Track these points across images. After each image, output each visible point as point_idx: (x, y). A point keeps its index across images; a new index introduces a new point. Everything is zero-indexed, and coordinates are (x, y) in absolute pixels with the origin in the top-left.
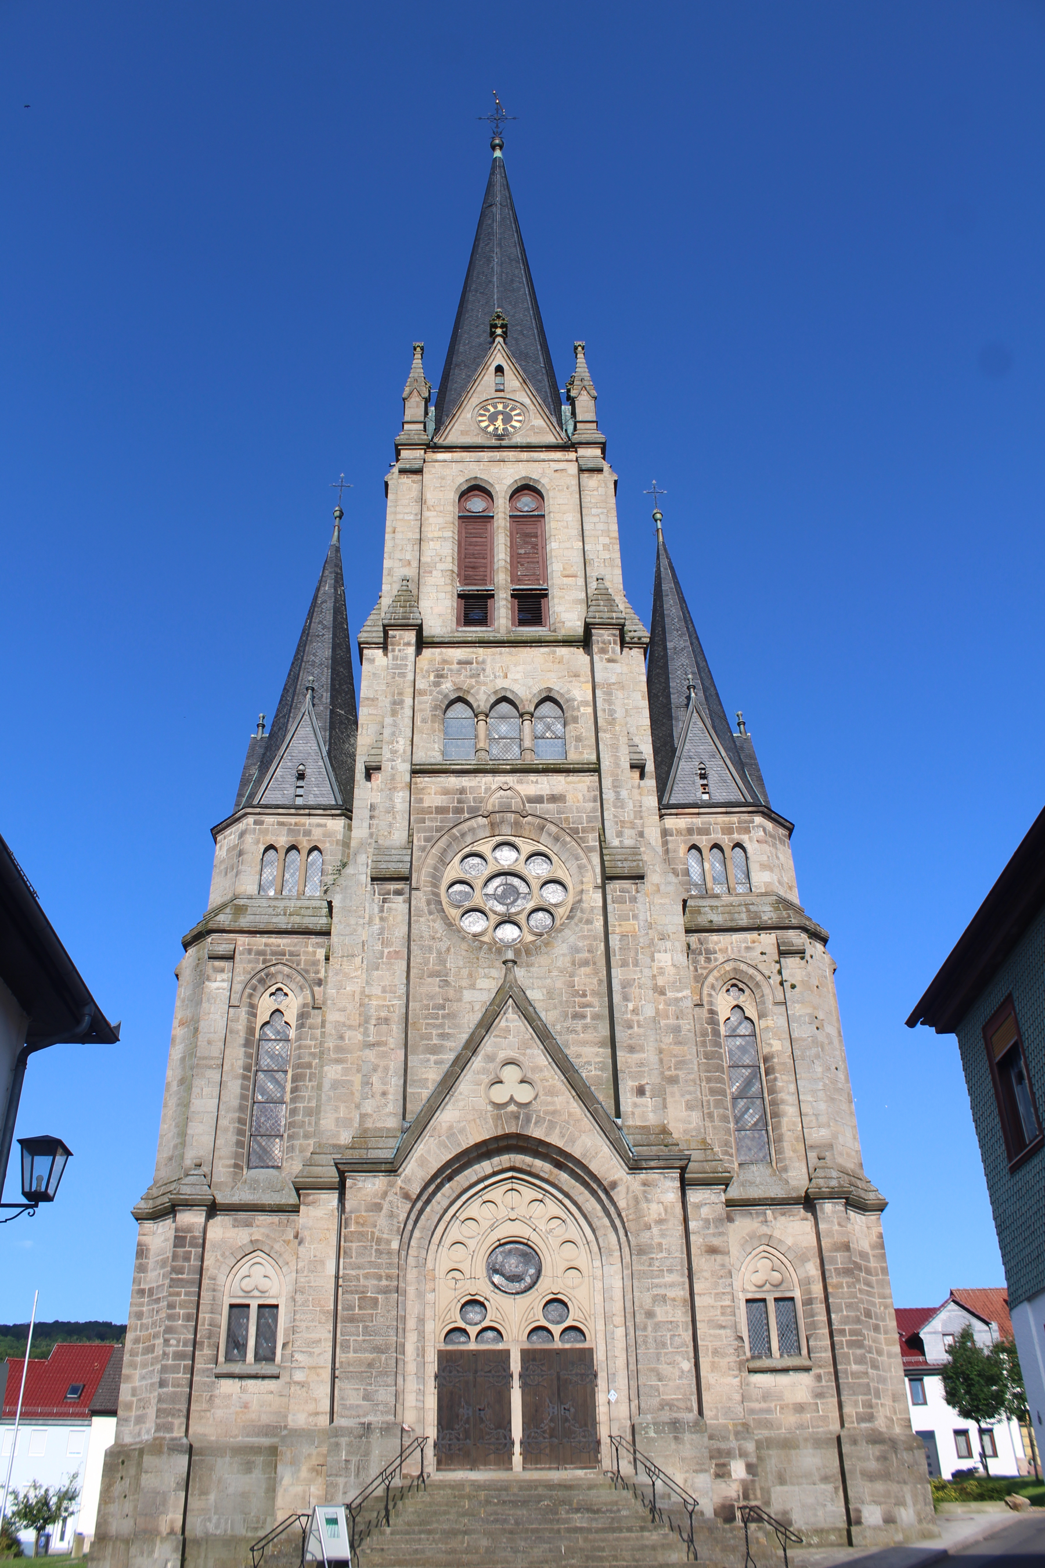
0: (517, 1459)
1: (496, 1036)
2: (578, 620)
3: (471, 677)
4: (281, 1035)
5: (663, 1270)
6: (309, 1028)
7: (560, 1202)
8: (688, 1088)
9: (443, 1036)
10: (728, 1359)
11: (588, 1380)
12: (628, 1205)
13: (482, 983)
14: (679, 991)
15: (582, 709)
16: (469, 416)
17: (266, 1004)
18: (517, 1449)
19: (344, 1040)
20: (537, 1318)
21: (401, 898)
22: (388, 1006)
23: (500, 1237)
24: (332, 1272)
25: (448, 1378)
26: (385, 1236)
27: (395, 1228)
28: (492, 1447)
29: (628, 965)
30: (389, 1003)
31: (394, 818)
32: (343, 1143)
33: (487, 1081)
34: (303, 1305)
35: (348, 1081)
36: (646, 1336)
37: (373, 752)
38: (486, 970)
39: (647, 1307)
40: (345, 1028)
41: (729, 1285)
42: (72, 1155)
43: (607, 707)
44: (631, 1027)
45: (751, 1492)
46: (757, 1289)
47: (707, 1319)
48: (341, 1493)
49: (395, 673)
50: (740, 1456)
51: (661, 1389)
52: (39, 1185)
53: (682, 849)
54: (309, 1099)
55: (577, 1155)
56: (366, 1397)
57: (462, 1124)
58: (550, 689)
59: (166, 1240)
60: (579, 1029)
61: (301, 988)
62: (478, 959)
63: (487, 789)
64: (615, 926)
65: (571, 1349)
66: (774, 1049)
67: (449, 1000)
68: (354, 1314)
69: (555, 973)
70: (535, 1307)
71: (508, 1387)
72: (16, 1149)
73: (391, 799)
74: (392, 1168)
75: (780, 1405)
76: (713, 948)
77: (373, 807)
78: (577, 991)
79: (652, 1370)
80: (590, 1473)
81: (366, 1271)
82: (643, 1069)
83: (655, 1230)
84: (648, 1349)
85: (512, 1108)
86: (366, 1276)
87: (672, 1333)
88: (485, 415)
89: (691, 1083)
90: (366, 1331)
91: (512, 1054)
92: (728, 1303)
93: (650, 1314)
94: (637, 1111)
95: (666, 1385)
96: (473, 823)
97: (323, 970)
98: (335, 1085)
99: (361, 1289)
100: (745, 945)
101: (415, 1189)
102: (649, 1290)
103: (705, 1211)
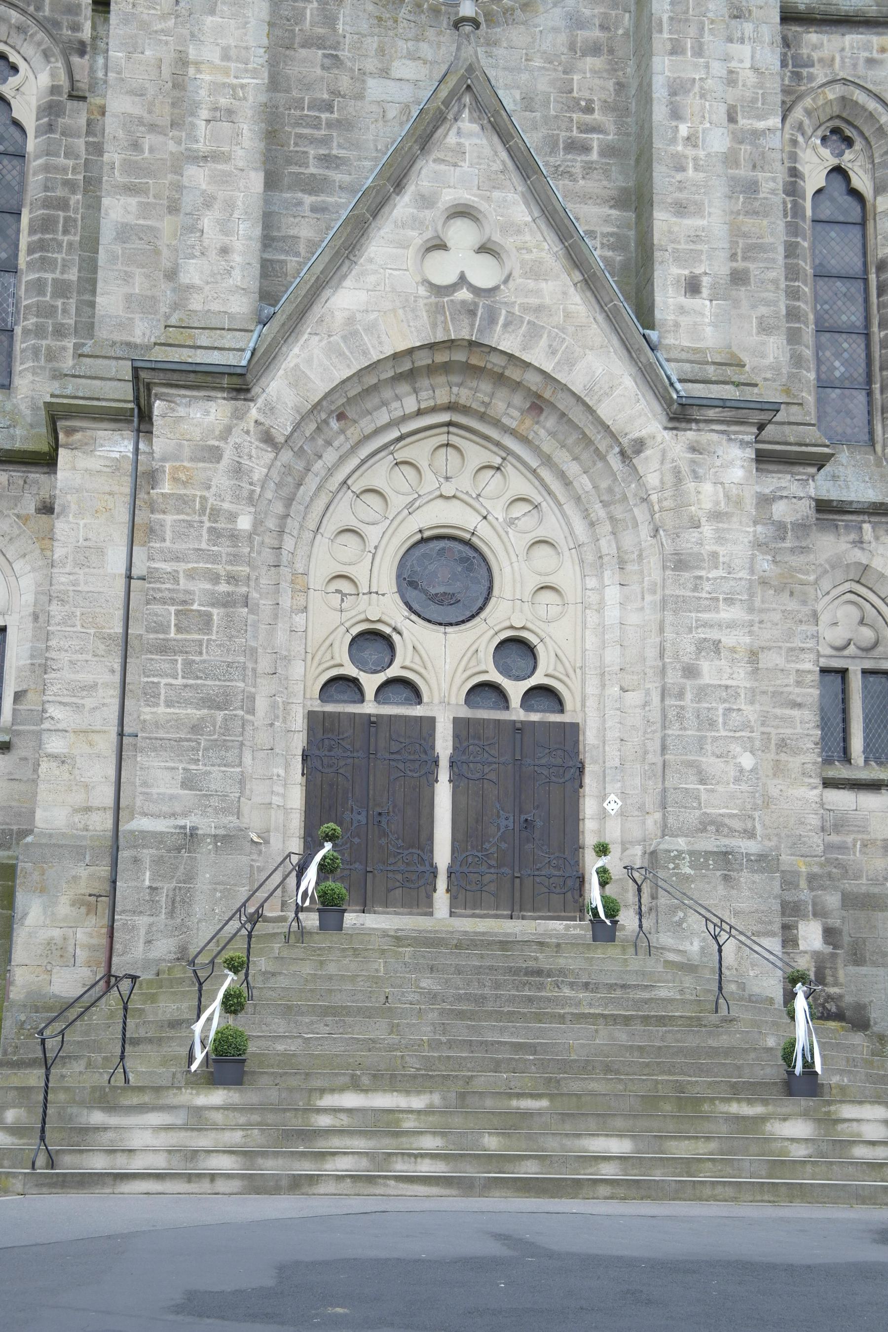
0: (441, 897)
4: (6, 143)
5: (717, 599)
6: (63, 134)
7: (534, 472)
8: (765, 295)
9: (327, 160)
10: (801, 759)
11: (567, 777)
12: (662, 482)
13: (404, 69)
14: (760, 118)
18: (442, 883)
19: (143, 152)
20: (483, 667)
22: (233, 87)
23: (422, 525)
24: (121, 569)
25: (325, 760)
26: (226, 506)
27: (245, 494)
28: (399, 877)
29: (683, 52)
30: (235, 81)
32: (138, 341)
33: (419, 241)
34: (64, 622)
35: (151, 228)
36: (682, 708)
38: (410, 43)
39: (686, 659)
40: (142, 129)
41: (813, 636)
44: (682, 169)
45: (828, 972)
46: (834, 653)
47: (771, 689)
48: (142, 941)
50: (815, 915)
51: (704, 797)
54: (64, 266)
55: (577, 389)
56: (188, 783)
57: (373, 316)
60: (577, 170)
62: (396, 21)
65: (541, 723)
67: (339, 95)
68: (167, 640)
69: (538, 63)
70: (482, 649)
75: (862, 840)
76: (809, 56)
78: (577, 101)
79: (690, 764)
80: (575, 927)
81: (190, 566)
82: (699, 247)
83: (707, 530)
84: (685, 729)
85: (464, 294)
86: (191, 575)
87: (727, 705)
89: (771, 287)
90: (189, 669)
91: (466, 196)
93: (690, 672)
94: (684, 320)
95: (713, 791)
97: (88, 26)
98: (124, 233)
99: (181, 596)
100: (866, 54)
101: (283, 426)
102: (690, 631)
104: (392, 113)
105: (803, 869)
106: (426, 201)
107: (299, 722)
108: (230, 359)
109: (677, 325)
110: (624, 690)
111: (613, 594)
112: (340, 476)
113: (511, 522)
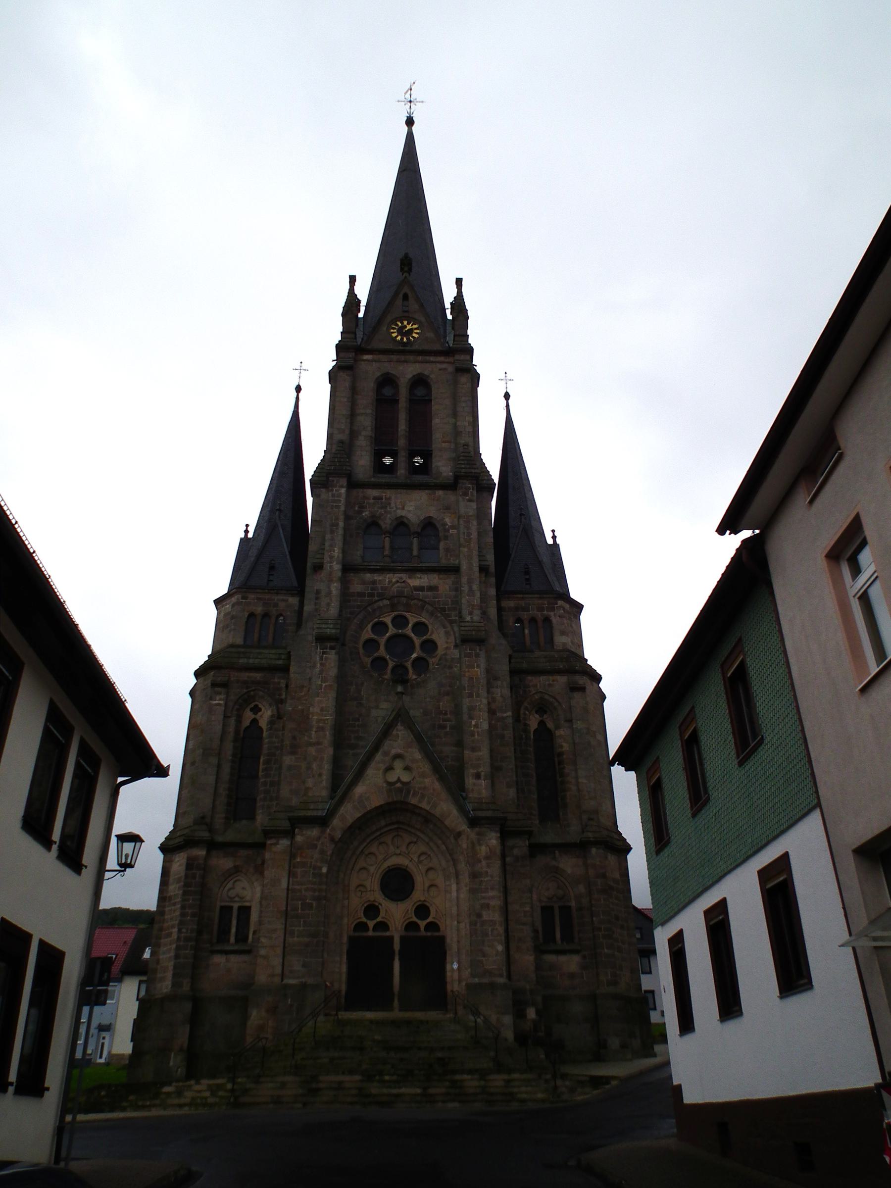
1: (390, 740)
2: (451, 472)
3: (381, 508)
5: (488, 888)
15: (451, 531)
16: (385, 329)
20: (410, 916)
21: (333, 652)
23: (389, 865)
31: (331, 600)
37: (318, 556)
42: (144, 841)
43: (466, 531)
44: (473, 735)
49: (332, 505)
52: (126, 859)
53: (511, 620)
58: (430, 517)
59: (180, 865)
61: (270, 705)
63: (390, 582)
64: (465, 671)
66: (564, 749)
71: (393, 959)
72: (114, 840)
73: (329, 587)
74: (323, 822)
77: (318, 592)
83: (484, 863)
88: (395, 329)
91: (399, 751)
92: (528, 909)
93: (479, 916)
96: (381, 604)
101: (338, 835)
103: (516, 851)
104: (380, 719)
105: (528, 987)
106: (386, 754)
107: (345, 939)
108: (319, 813)
109: (473, 790)
110: (458, 922)
111: (454, 887)
112: (360, 850)
113: (420, 862)
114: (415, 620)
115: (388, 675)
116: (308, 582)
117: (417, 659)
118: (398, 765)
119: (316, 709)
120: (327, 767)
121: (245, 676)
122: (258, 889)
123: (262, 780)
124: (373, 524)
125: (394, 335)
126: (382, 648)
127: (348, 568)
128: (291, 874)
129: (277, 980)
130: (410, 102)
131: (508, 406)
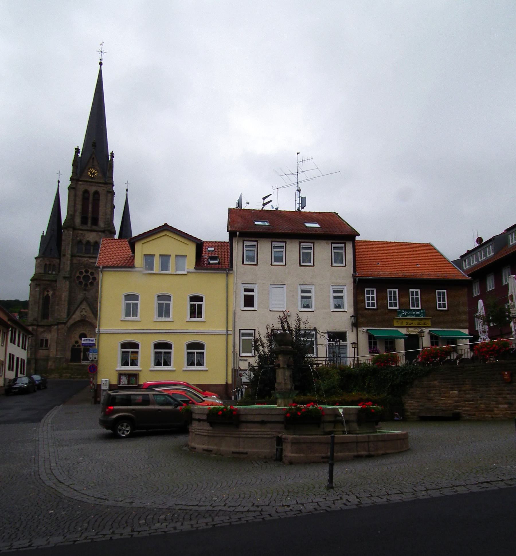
17: (46, 293)
58: (97, 241)
74: (65, 323)
77: (64, 263)
91: (84, 308)
96: (81, 267)
101: (69, 326)
107: (70, 348)
114: (91, 271)
115: (83, 286)
116: (62, 259)
117: (91, 282)
118: (84, 311)
119: (63, 296)
120: (66, 311)
121: (45, 282)
122: (50, 336)
123: (50, 310)
124: (80, 242)
125: (89, 174)
126: (82, 278)
127: (72, 256)
128: (58, 334)
129: (55, 356)
130: (102, 52)
131: (127, 194)
